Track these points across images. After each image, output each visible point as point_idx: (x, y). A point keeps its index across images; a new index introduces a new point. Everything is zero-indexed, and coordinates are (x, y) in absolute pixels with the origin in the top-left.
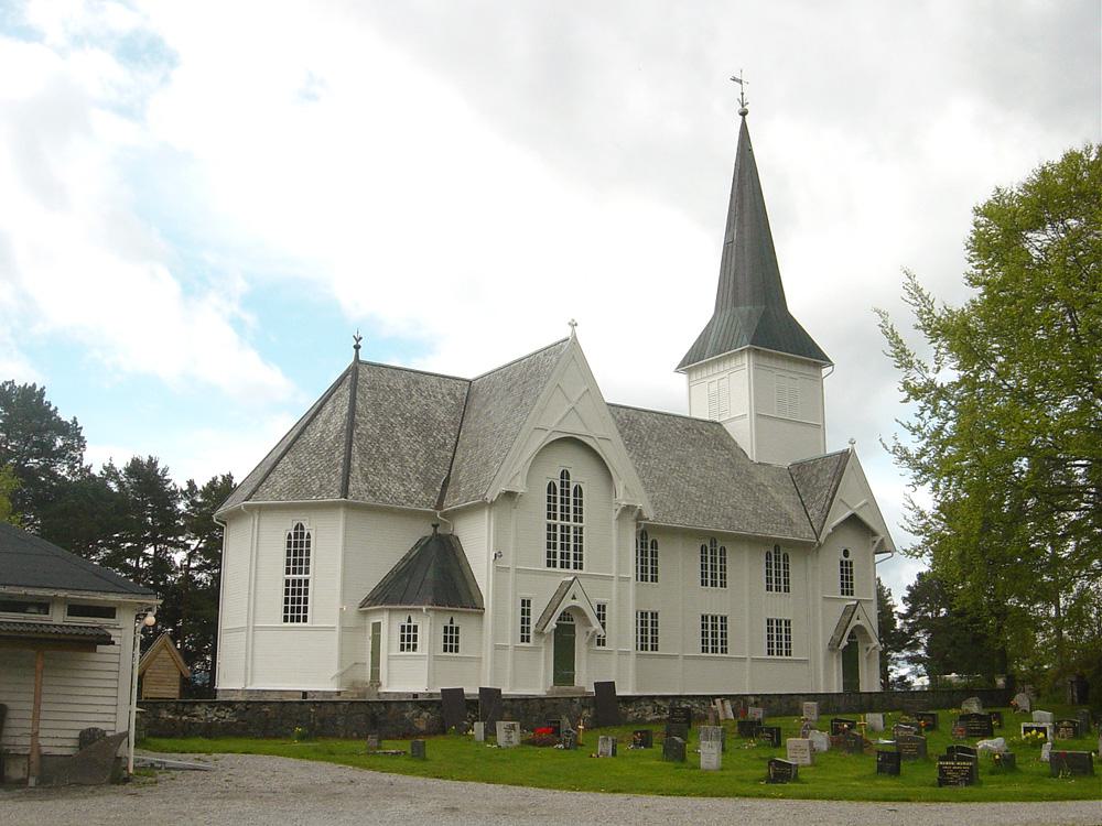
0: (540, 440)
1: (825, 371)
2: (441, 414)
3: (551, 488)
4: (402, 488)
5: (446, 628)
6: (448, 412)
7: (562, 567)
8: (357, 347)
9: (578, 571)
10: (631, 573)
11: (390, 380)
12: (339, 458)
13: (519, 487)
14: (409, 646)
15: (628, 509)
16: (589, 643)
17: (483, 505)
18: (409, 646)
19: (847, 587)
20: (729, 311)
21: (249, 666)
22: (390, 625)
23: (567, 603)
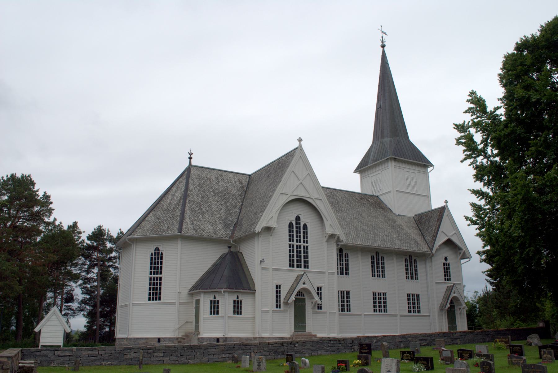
0: (284, 199)
1: (429, 169)
3: (291, 225)
5: (234, 301)
7: (297, 267)
8: (190, 158)
9: (306, 269)
15: (332, 236)
18: (214, 312)
19: (447, 277)
23: (300, 286)
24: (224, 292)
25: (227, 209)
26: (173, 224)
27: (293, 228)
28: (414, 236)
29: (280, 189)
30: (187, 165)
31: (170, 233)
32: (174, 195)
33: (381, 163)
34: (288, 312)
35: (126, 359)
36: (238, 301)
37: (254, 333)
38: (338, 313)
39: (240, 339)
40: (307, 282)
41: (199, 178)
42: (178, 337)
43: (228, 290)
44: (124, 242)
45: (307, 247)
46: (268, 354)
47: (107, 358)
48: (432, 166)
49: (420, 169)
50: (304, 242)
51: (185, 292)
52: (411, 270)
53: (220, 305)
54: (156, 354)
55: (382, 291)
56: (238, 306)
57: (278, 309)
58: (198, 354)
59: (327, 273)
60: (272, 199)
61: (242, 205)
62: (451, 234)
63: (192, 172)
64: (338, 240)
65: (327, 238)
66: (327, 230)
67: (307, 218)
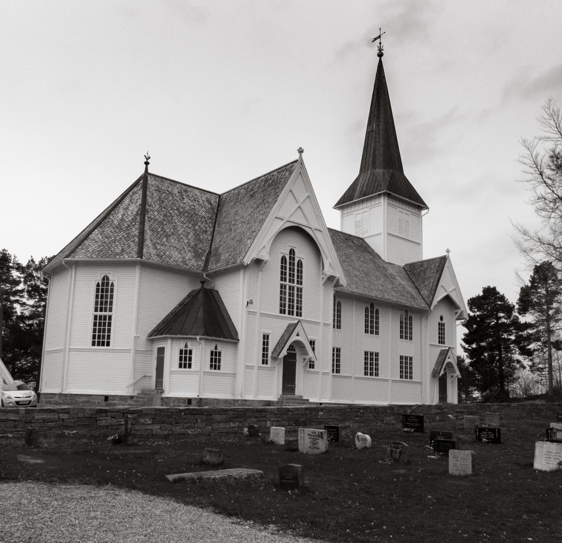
0: (279, 225)
1: (423, 212)
2: (202, 212)
3: (283, 259)
4: (179, 255)
5: (212, 352)
6: (207, 212)
7: (289, 314)
8: (147, 163)
9: (299, 318)
10: (331, 322)
11: (169, 187)
12: (135, 231)
13: (264, 256)
14: (185, 364)
15: (331, 279)
16: (305, 366)
17: (242, 267)
18: (185, 364)
19: (442, 340)
20: (369, 172)
21: (65, 377)
22: (172, 350)
23: (294, 338)
24: (200, 339)
25: (197, 235)
26: (129, 246)
27: (286, 264)
28: (410, 289)
29: (275, 211)
30: (142, 172)
31: (126, 258)
32: (127, 208)
33: (371, 199)
34: (276, 369)
35: (100, 427)
36: (216, 352)
37: (234, 394)
38: (331, 374)
39: (218, 401)
40: (301, 333)
41: (158, 190)
42: (132, 395)
43: (206, 337)
44: (54, 268)
45: (301, 289)
46: (287, 423)
47: (70, 425)
48: (428, 208)
49: (414, 210)
50: (298, 283)
51: (144, 337)
52: (406, 328)
53: (193, 356)
54: (142, 420)
55: (374, 350)
56: (216, 359)
57: (264, 365)
58: (199, 421)
59: (322, 324)
60: (265, 224)
61: (214, 230)
62: (451, 289)
63: (149, 182)
64: (337, 285)
65: (324, 280)
66: (325, 270)
67: (303, 253)
